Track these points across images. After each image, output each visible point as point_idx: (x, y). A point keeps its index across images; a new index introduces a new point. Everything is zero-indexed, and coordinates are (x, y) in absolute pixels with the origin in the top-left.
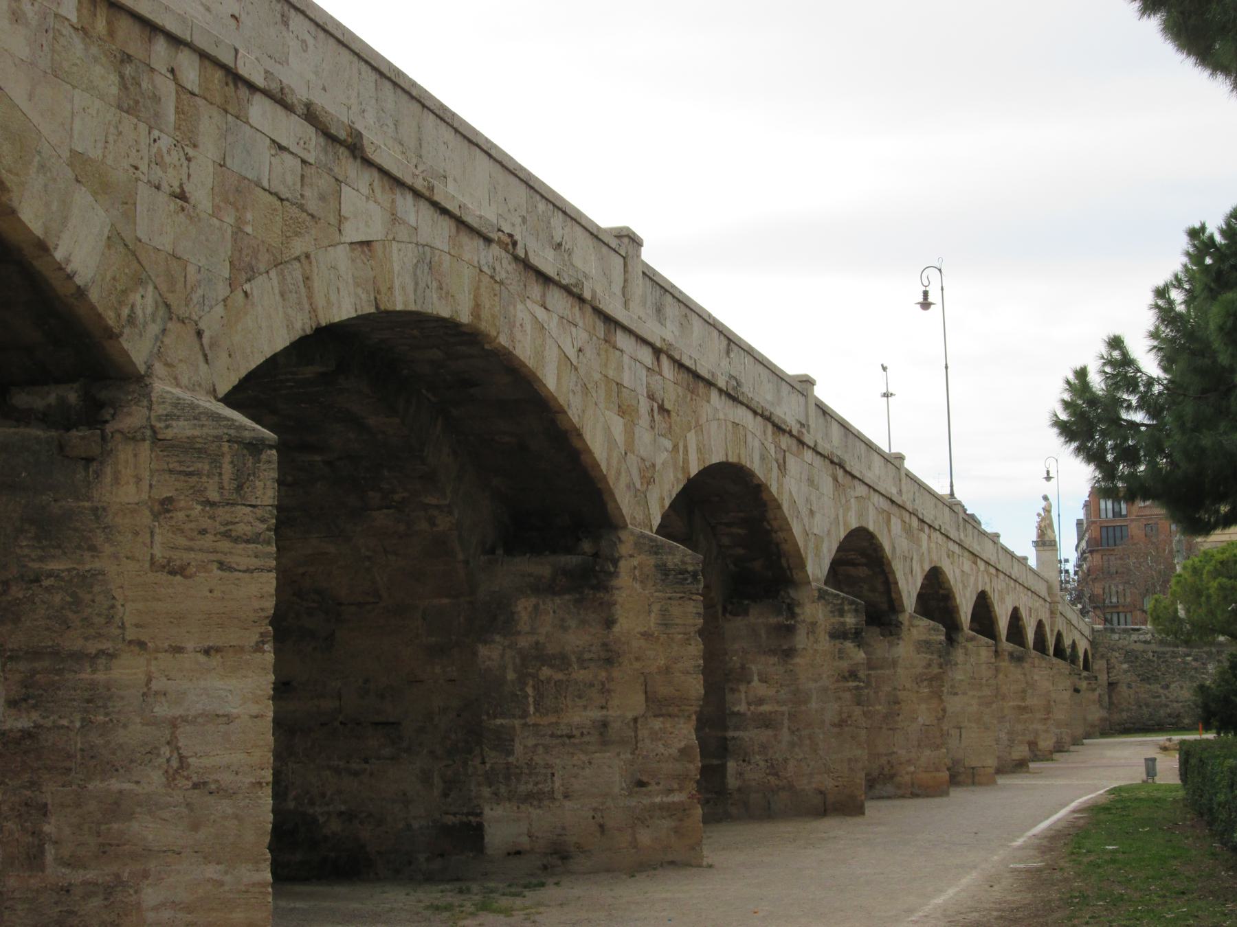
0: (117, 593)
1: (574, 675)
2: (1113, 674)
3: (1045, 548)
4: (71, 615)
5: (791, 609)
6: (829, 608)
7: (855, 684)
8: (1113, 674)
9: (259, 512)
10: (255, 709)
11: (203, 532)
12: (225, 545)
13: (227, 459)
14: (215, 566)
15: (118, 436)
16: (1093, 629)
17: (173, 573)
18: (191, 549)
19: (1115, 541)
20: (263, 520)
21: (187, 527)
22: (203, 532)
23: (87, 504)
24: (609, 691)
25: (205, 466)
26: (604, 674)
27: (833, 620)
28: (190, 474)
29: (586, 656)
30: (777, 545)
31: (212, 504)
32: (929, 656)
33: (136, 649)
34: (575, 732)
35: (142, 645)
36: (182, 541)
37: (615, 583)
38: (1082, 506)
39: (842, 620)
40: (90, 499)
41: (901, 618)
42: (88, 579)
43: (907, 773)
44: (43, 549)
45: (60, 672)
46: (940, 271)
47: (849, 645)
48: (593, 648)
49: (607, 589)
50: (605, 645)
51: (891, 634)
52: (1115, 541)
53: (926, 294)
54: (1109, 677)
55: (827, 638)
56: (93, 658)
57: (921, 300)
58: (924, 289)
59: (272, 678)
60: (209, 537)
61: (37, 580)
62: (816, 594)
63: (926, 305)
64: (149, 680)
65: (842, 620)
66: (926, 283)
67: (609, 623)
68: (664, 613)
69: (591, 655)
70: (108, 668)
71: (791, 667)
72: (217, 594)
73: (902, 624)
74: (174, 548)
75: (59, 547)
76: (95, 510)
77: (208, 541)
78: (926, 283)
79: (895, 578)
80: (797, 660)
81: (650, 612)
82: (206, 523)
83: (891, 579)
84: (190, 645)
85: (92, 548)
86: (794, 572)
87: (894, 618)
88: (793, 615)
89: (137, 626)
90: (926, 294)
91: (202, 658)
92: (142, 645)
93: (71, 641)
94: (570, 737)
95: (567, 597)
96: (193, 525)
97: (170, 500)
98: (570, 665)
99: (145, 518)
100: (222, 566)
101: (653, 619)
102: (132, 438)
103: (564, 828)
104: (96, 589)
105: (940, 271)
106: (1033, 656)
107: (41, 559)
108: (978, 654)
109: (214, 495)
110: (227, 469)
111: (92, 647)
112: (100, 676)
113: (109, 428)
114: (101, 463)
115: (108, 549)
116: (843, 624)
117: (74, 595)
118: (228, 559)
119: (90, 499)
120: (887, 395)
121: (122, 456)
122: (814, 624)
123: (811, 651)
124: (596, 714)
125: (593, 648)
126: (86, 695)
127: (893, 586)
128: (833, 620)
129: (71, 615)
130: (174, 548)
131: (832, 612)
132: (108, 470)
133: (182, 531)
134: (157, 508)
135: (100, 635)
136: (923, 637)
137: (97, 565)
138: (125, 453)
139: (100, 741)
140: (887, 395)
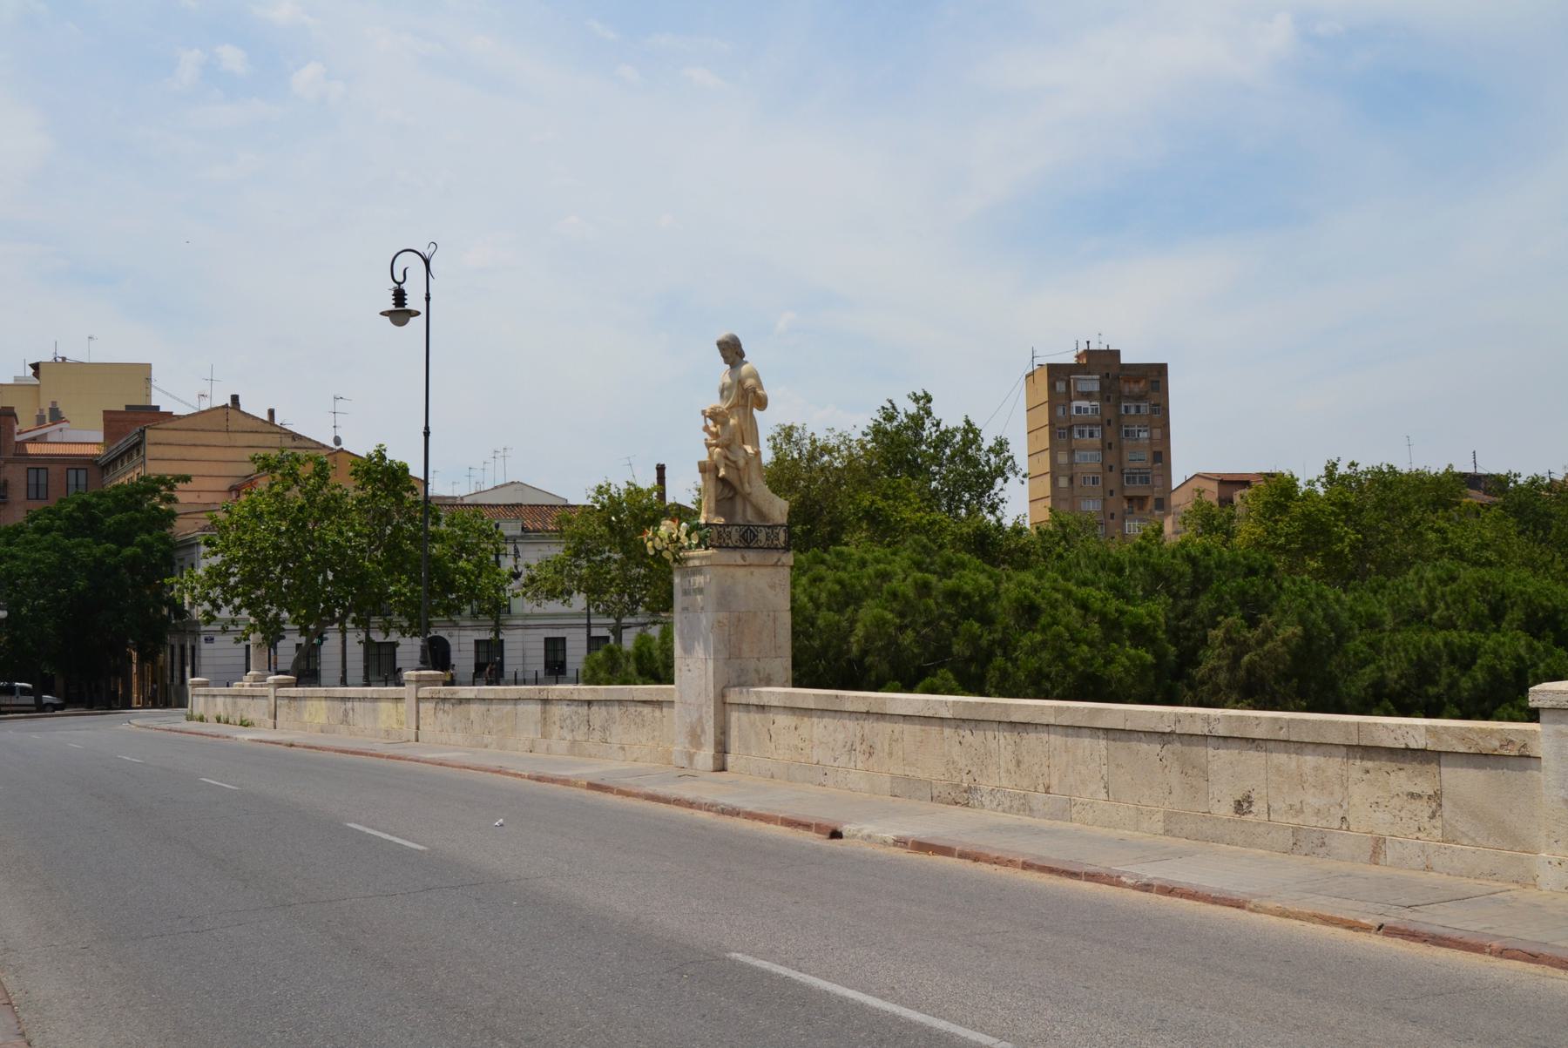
46: (427, 262)
57: (390, 305)
105: (427, 262)
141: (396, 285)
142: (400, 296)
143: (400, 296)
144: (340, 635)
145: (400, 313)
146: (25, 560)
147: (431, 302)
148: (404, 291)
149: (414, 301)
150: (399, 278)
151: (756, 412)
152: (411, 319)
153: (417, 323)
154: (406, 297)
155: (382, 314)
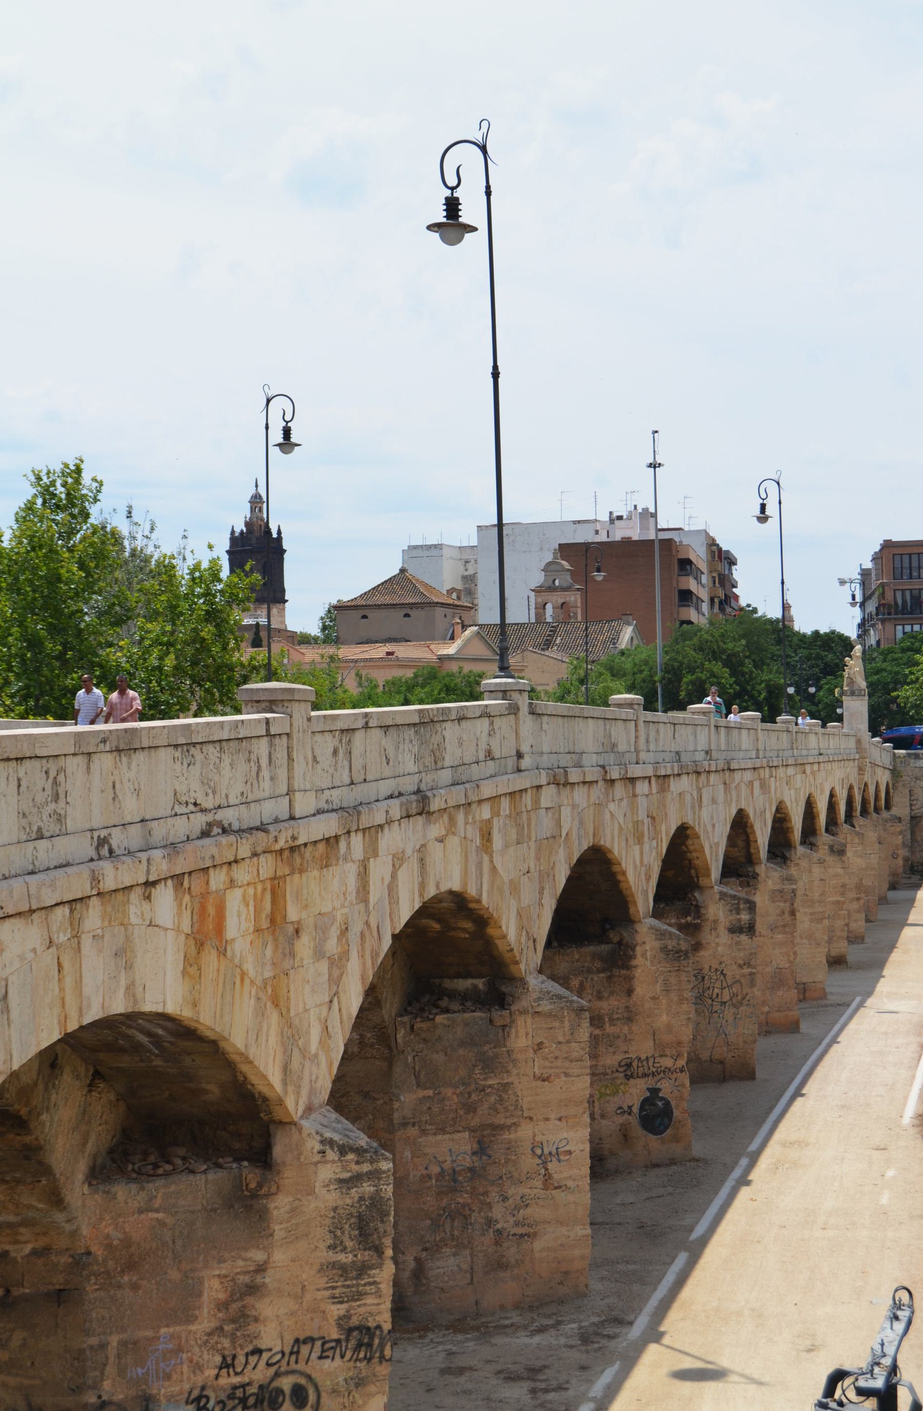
0: (519, 1093)
1: (607, 1031)
2: (917, 807)
3: (854, 698)
4: (499, 1106)
5: (697, 910)
6: (728, 907)
7: (749, 970)
8: (917, 807)
9: (582, 1045)
10: (581, 1147)
11: (556, 1058)
12: (567, 1064)
13: (567, 1019)
14: (562, 1075)
15: (517, 1013)
16: (894, 754)
17: (544, 1080)
18: (551, 1068)
19: (911, 574)
20: (583, 1049)
21: (549, 1056)
22: (556, 1058)
23: (504, 1049)
24: (630, 1040)
25: (557, 1024)
26: (626, 1028)
27: (731, 918)
28: (551, 1028)
29: (615, 1016)
30: (690, 861)
31: (560, 1043)
32: (781, 904)
33: (528, 1120)
34: (609, 1071)
35: (531, 1119)
36: (547, 1064)
37: (634, 963)
38: (871, 558)
39: (738, 917)
40: (505, 1046)
41: (758, 870)
42: (506, 1086)
43: (762, 1013)
44: (485, 1074)
45: (494, 1136)
46: (778, 483)
47: (744, 938)
48: (620, 1011)
49: (628, 968)
50: (627, 1007)
51: (748, 885)
52: (911, 574)
53: (763, 507)
54: (912, 810)
55: (726, 932)
56: (509, 1127)
57: (757, 512)
58: (761, 501)
59: (589, 1130)
60: (560, 1061)
61: (484, 1090)
62: (717, 896)
63: (763, 517)
64: (535, 1136)
65: (738, 917)
66: (764, 496)
67: (630, 992)
68: (666, 982)
69: (618, 1016)
70: (516, 1132)
71: (697, 959)
72: (564, 1088)
73: (758, 875)
74: (544, 1068)
75: (493, 1072)
76: (508, 1052)
77: (559, 1063)
78: (764, 496)
79: (755, 837)
80: (702, 953)
81: (657, 982)
82: (557, 1053)
83: (751, 838)
84: (552, 1116)
85: (508, 1072)
86: (701, 879)
87: (750, 869)
88: (698, 915)
89: (529, 1109)
90: (763, 507)
91: (558, 1123)
92: (531, 1119)
93: (500, 1120)
94: (605, 1074)
95: (602, 975)
96: (552, 1055)
97: (542, 1043)
98: (604, 1023)
99: (531, 1053)
100: (566, 1075)
101: (659, 987)
102: (524, 1012)
103: (600, 1139)
104: (510, 1092)
105: (778, 483)
106: (845, 831)
107: (485, 1079)
108: (810, 871)
109: (561, 1039)
110: (567, 1024)
111: (509, 1122)
112: (512, 1136)
113: (513, 1008)
114: (510, 1027)
115: (515, 1071)
116: (739, 920)
117: (500, 1096)
118: (568, 1071)
119: (505, 1046)
120: (654, 466)
121: (519, 1023)
122: (716, 921)
123: (714, 945)
124: (619, 1057)
125: (620, 1011)
126: (507, 1146)
127: (752, 843)
128: (731, 918)
129: (499, 1106)
130: (544, 1068)
131: (731, 911)
132: (513, 1030)
133: (547, 1059)
134: (536, 1047)
135: (512, 1115)
136: (778, 887)
137: (510, 1080)
138: (520, 1021)
139: (513, 1169)
140: (654, 466)
141: (448, 193)
142: (452, 206)
143: (452, 206)
144: (504, 522)
145: (763, 517)
146: (890, 672)
147: (492, 197)
148: (457, 199)
149: (472, 212)
150: (452, 182)
151: (734, 590)
152: (467, 235)
153: (474, 243)
154: (460, 207)
155: (429, 228)
